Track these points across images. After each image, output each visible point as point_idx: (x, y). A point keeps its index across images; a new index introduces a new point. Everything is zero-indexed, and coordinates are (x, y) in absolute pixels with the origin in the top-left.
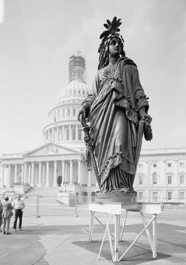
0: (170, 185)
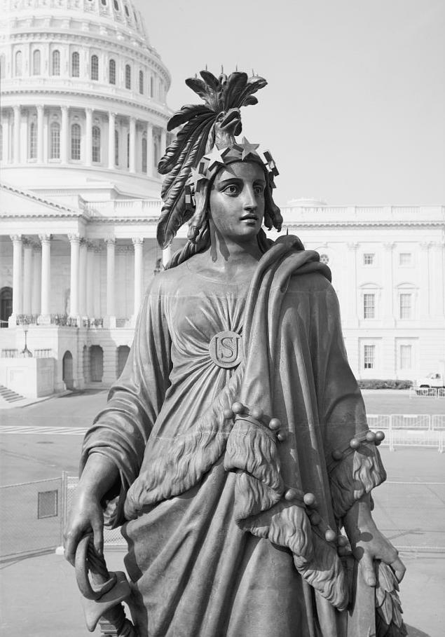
0: (367, 323)
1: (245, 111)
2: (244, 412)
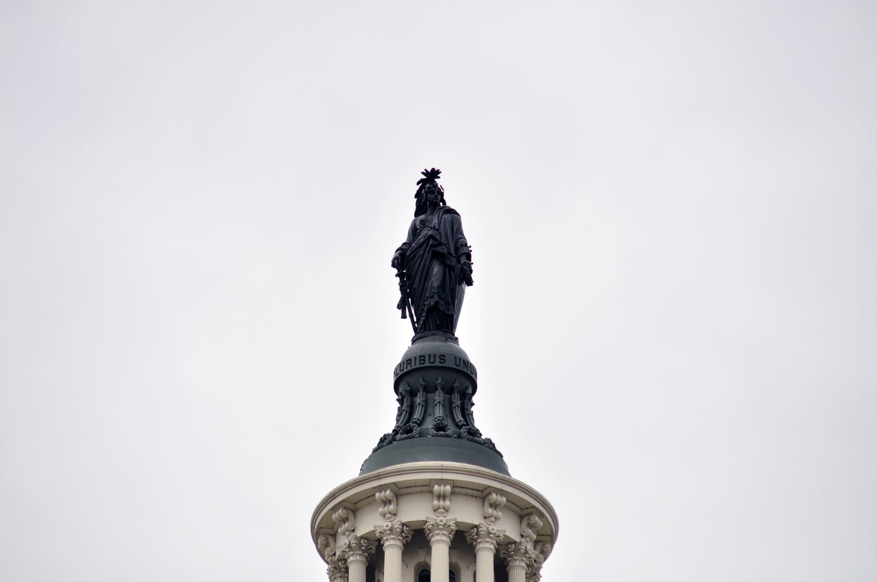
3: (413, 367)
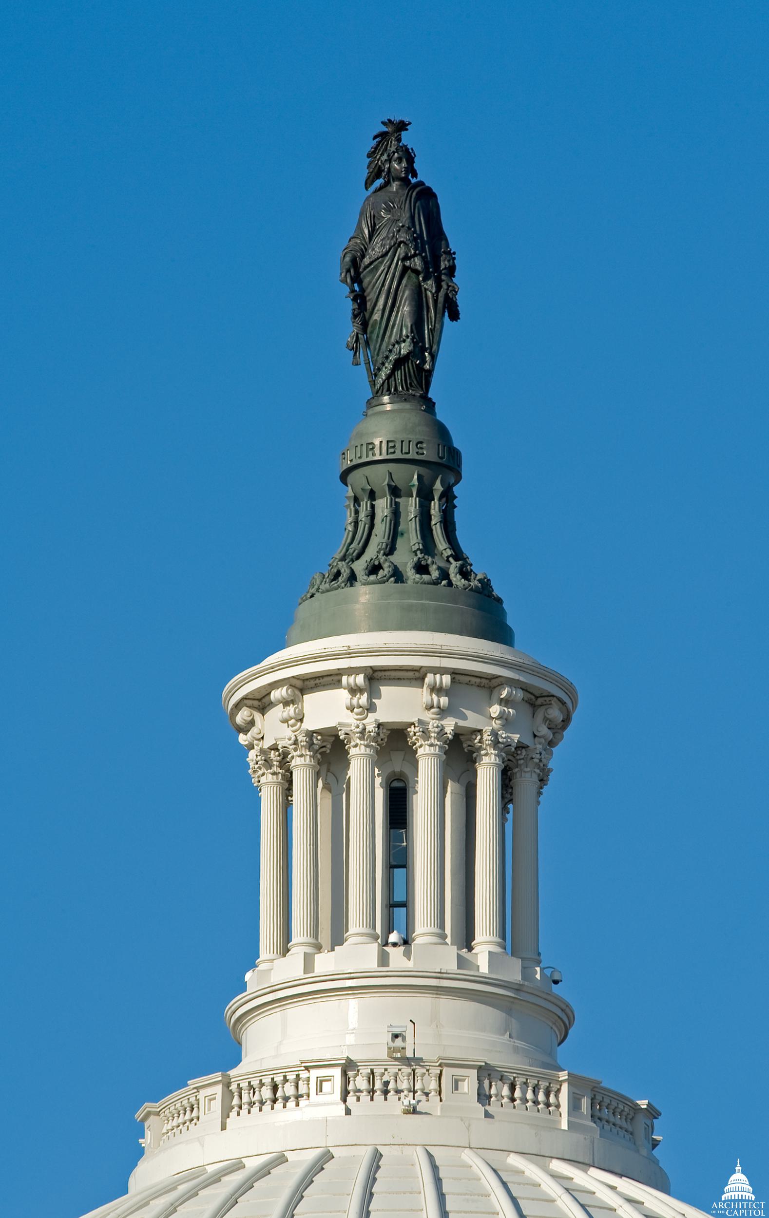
1: (403, 133)
2: (403, 226)
3: (378, 457)
